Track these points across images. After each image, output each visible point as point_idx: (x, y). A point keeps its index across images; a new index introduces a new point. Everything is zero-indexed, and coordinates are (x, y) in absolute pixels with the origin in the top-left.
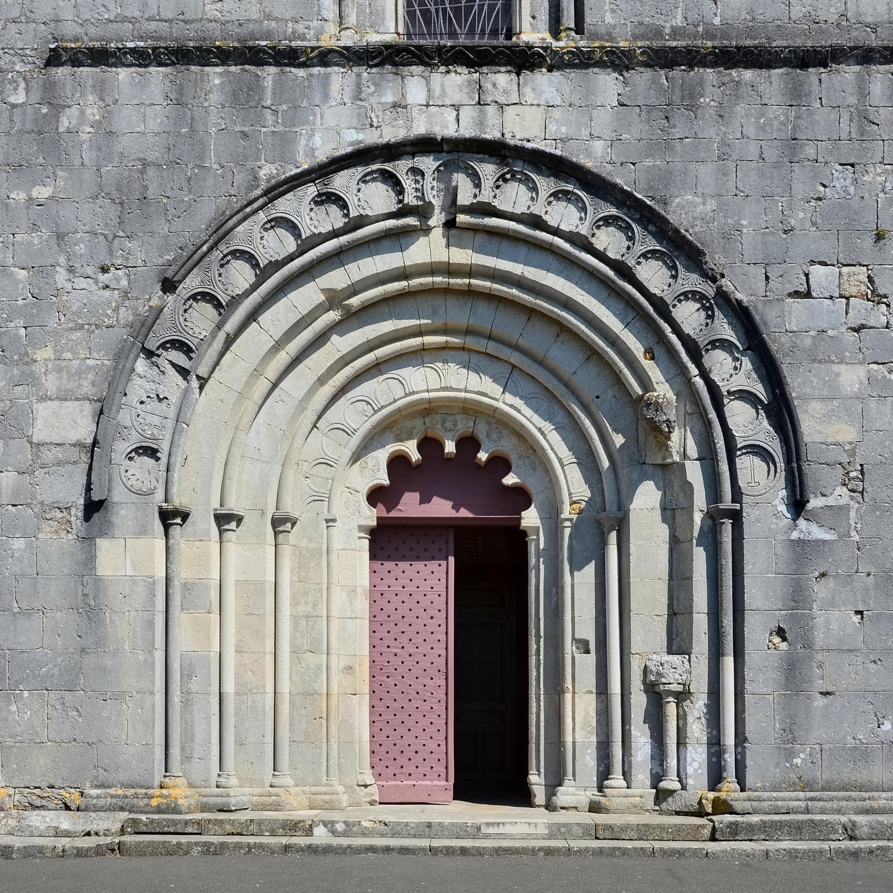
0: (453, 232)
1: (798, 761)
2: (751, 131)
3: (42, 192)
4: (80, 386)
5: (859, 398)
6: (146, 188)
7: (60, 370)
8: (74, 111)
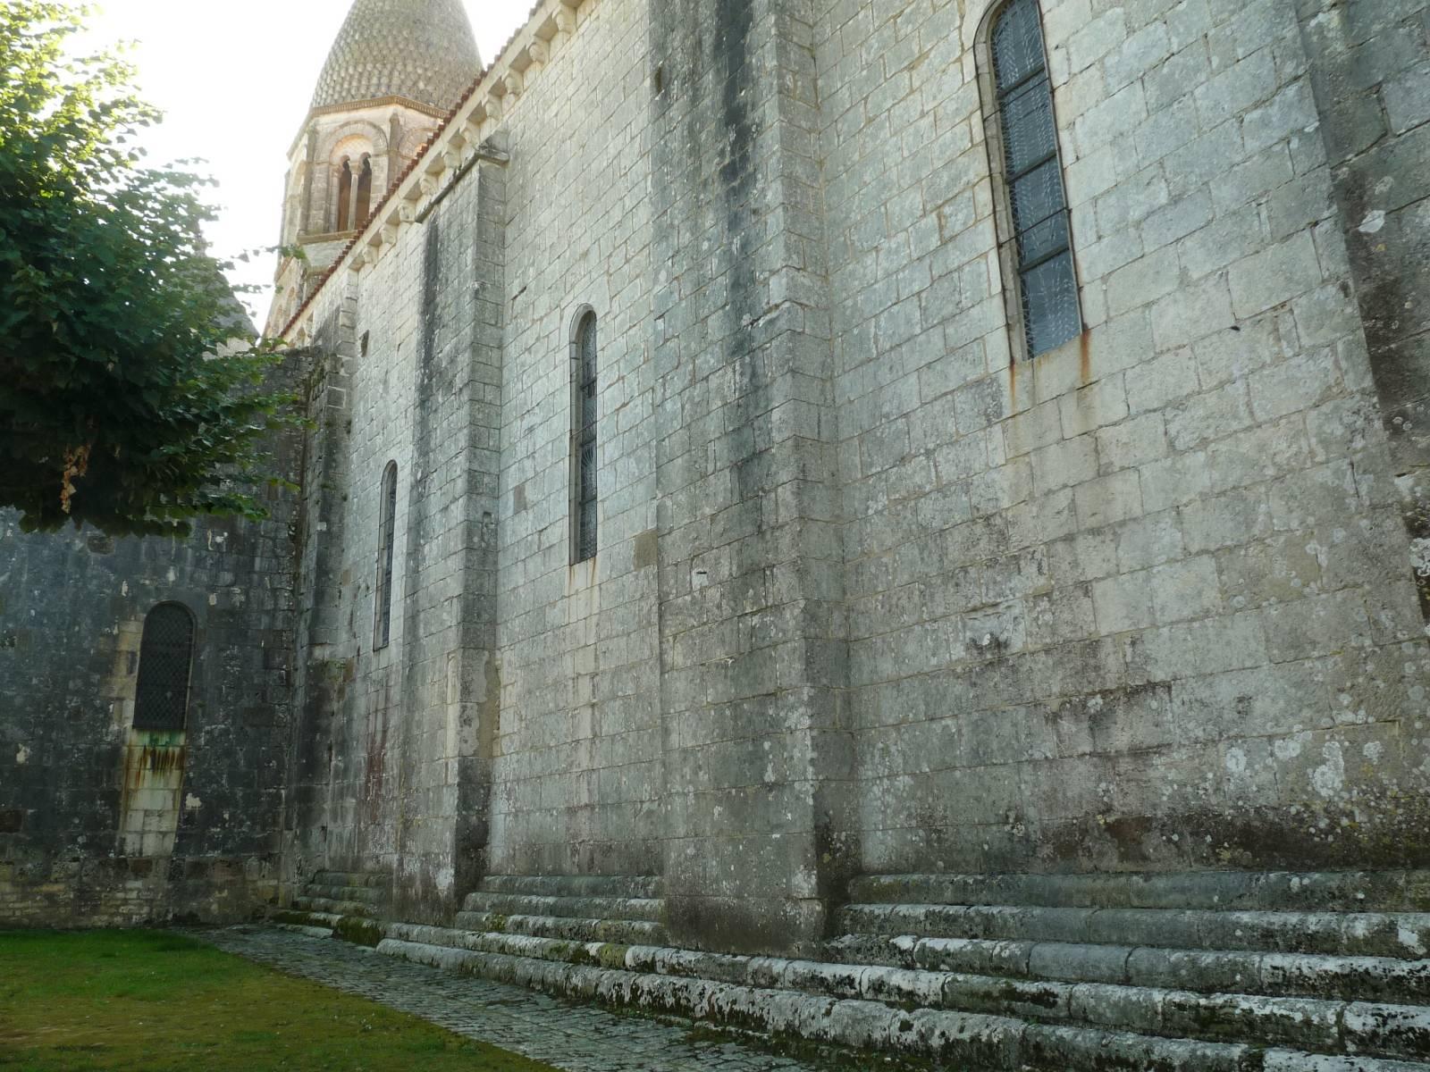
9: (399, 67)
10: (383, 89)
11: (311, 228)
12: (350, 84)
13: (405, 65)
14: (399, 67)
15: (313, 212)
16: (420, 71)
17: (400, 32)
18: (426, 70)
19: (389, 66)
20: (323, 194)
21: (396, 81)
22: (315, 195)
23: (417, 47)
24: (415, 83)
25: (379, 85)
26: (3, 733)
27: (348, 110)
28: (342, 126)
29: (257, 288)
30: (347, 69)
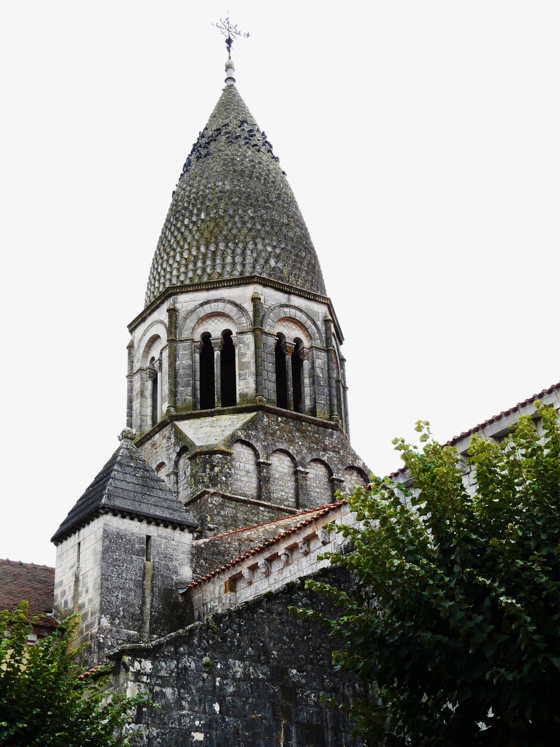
9: (251, 246)
10: (239, 268)
11: (179, 404)
12: (204, 263)
13: (256, 244)
14: (251, 246)
15: (180, 389)
16: (269, 249)
17: (245, 211)
18: (274, 247)
19: (241, 245)
20: (189, 372)
21: (249, 260)
22: (181, 372)
23: (263, 226)
24: (267, 261)
25: (234, 264)
26: (1, 668)
27: (208, 290)
28: (202, 305)
29: (229, 67)
30: (198, 249)
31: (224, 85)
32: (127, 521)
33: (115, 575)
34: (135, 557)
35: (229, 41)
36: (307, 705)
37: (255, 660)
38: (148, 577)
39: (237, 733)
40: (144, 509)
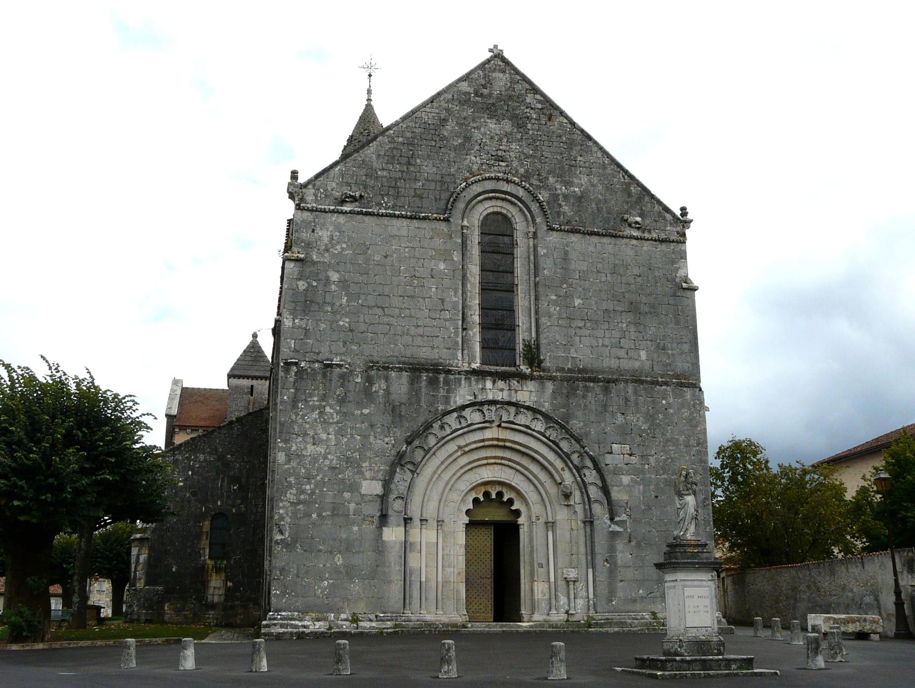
0: (500, 428)
1: (614, 603)
2: (593, 402)
3: (366, 411)
4: (378, 476)
5: (628, 486)
6: (401, 412)
7: (371, 470)
8: (377, 385)
31: (366, 103)
32: (241, 380)
33: (234, 405)
34: (244, 396)
35: (370, 75)
36: (234, 468)
37: (210, 454)
38: (251, 404)
39: (199, 482)
40: (250, 373)
